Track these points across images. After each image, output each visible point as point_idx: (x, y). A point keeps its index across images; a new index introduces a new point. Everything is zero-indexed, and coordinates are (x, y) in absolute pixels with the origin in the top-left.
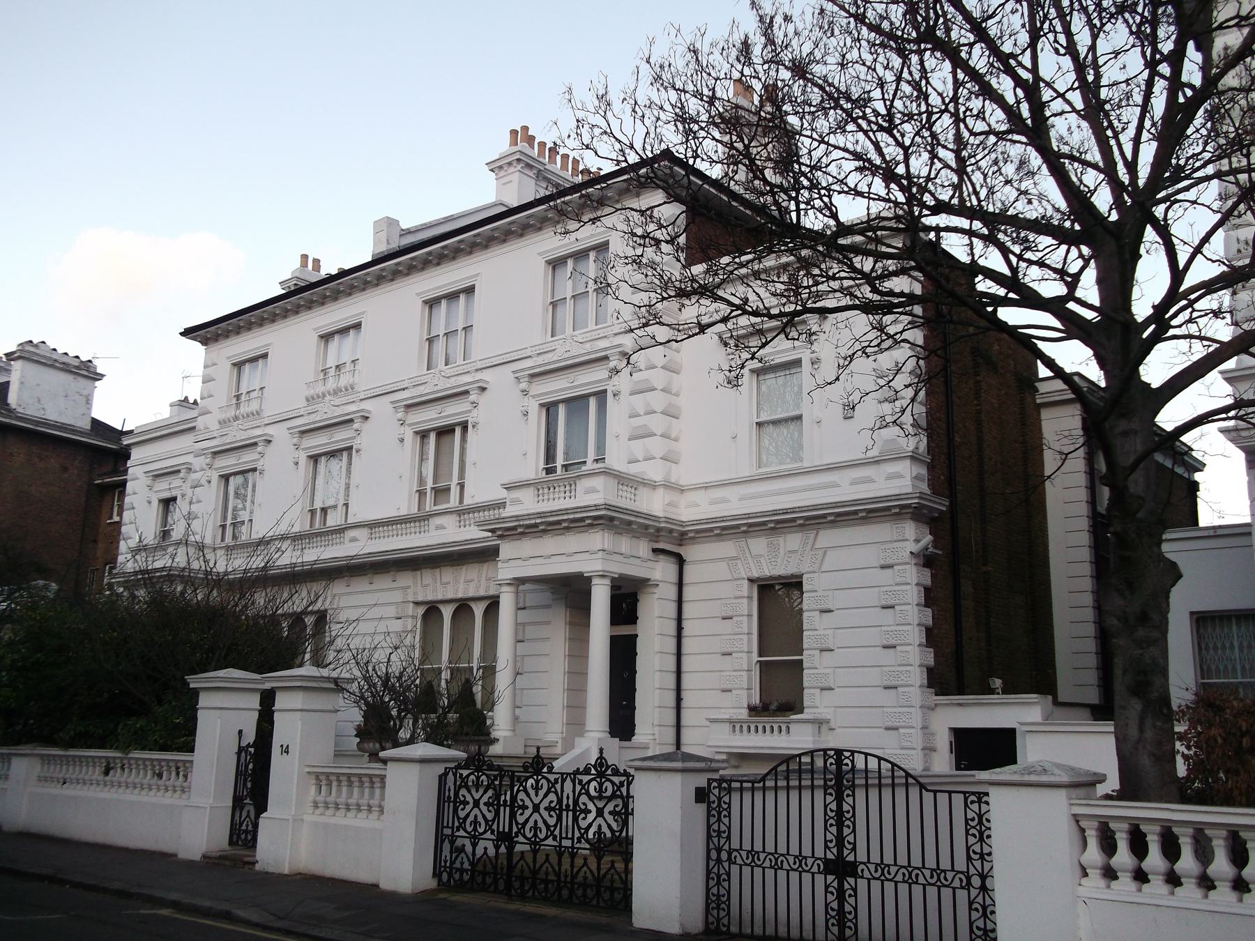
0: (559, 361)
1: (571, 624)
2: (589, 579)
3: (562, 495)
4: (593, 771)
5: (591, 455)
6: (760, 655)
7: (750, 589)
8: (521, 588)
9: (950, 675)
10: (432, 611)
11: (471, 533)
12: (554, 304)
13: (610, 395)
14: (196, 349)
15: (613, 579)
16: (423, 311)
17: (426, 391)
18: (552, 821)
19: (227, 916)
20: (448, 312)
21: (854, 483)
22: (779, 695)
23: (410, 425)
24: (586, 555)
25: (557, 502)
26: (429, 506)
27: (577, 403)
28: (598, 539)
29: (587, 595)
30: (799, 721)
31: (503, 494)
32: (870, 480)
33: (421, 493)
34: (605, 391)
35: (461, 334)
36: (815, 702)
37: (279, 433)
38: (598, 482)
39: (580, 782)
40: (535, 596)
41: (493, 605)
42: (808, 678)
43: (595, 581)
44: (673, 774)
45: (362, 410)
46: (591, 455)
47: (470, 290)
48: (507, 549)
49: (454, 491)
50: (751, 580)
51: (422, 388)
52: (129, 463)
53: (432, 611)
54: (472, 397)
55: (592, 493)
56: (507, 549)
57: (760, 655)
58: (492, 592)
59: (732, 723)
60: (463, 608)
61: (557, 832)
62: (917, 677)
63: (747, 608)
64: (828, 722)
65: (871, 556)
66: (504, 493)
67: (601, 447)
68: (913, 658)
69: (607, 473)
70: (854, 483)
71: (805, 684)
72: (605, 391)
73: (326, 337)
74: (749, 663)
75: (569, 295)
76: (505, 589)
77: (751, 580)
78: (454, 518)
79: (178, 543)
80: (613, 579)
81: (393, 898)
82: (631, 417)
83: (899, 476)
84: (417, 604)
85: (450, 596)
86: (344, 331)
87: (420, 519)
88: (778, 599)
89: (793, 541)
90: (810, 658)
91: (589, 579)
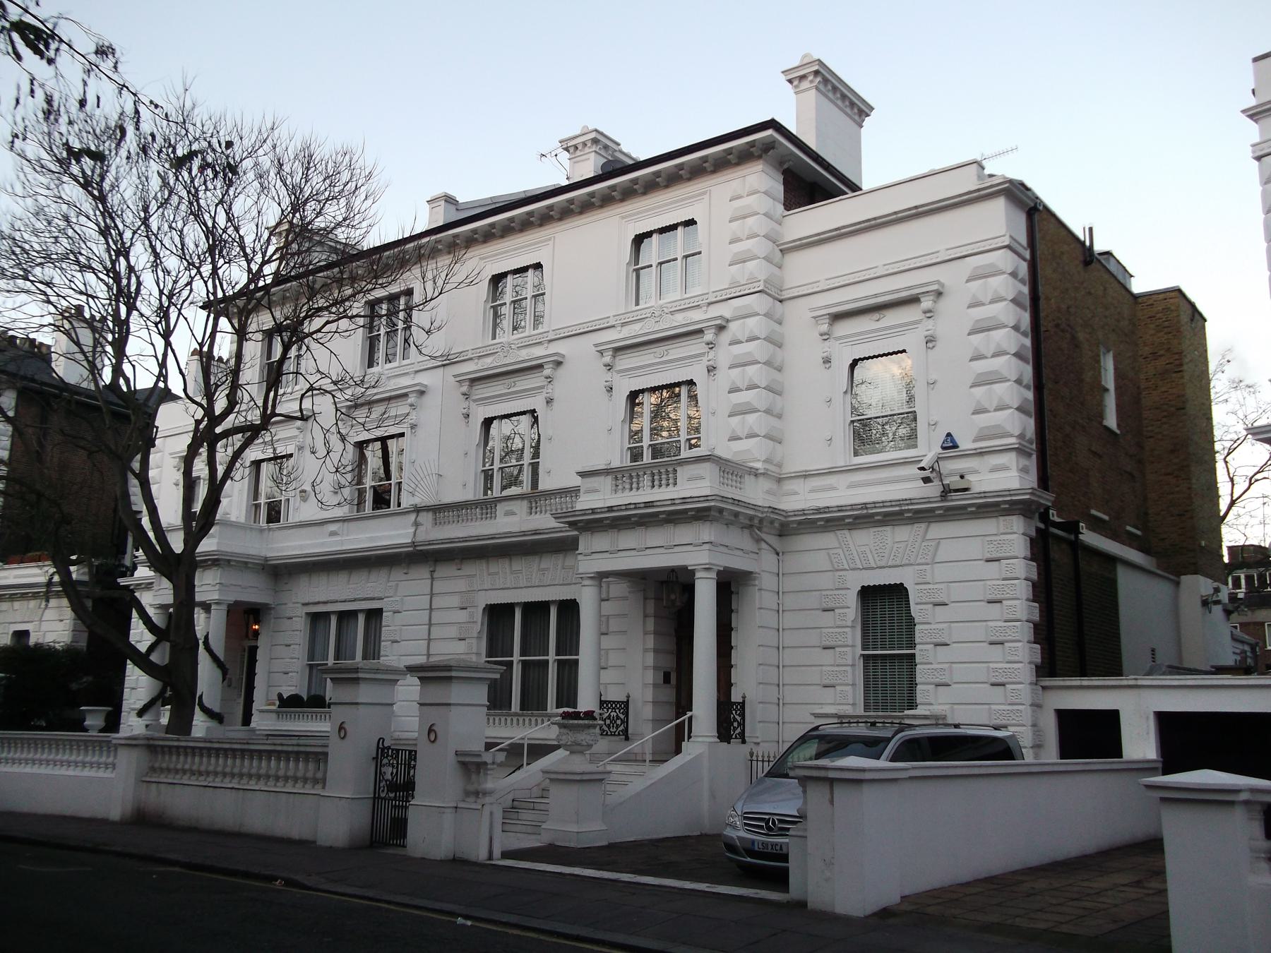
0: (634, 337)
2: (693, 572)
6: (863, 649)
9: (1051, 666)
10: (498, 615)
11: (545, 522)
15: (229, 606)
25: (646, 494)
26: (496, 492)
28: (706, 532)
29: (689, 589)
31: (577, 481)
33: (488, 476)
37: (579, 352)
40: (619, 588)
42: (921, 672)
43: (698, 575)
48: (588, 543)
49: (526, 477)
53: (498, 615)
54: (547, 372)
55: (694, 485)
57: (863, 649)
60: (535, 611)
62: (1025, 672)
65: (975, 548)
66: (577, 481)
68: (1022, 654)
71: (918, 680)
74: (854, 659)
78: (525, 504)
80: (719, 573)
83: (1004, 468)
87: (486, 506)
90: (922, 651)
91: (693, 572)
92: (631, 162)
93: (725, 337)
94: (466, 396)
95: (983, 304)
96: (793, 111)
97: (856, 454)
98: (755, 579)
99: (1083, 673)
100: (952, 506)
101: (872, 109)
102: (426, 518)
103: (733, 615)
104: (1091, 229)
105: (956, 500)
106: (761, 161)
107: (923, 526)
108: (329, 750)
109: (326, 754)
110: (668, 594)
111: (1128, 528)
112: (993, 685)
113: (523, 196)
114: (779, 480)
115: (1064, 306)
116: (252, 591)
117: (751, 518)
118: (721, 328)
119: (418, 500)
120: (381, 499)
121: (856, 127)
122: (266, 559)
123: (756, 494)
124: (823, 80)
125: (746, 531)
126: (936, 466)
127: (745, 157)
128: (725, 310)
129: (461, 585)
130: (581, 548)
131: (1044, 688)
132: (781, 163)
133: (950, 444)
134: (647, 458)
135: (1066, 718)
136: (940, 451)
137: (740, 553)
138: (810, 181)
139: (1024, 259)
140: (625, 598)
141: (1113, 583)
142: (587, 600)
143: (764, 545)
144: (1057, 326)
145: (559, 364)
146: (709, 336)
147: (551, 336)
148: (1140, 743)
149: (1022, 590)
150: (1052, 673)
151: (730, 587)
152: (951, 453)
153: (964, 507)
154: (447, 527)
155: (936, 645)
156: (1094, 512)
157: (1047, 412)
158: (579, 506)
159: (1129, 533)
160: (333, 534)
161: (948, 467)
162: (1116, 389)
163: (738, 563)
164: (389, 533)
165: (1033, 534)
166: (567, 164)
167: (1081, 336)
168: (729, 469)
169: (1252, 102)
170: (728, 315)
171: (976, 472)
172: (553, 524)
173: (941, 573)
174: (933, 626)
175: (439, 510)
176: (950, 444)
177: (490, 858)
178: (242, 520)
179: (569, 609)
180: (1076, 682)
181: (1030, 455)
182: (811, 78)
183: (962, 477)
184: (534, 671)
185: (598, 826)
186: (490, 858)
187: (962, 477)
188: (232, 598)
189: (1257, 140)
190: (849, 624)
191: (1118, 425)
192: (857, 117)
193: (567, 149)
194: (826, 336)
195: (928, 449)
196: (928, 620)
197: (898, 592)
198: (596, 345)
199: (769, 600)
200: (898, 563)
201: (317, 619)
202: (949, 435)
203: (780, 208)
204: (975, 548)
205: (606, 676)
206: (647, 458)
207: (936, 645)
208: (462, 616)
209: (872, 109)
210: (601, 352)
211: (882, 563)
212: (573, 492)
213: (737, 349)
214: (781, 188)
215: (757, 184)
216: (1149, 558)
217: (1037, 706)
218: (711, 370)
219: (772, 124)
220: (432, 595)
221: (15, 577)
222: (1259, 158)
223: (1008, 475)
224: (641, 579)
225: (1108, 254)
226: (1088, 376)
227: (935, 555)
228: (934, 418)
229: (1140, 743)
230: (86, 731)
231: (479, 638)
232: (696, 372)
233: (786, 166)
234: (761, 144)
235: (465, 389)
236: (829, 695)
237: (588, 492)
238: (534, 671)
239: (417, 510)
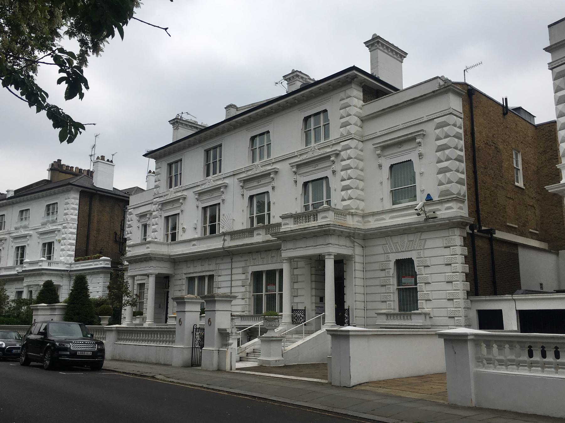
2: (324, 256)
5: (325, 200)
9: (475, 291)
10: (257, 276)
15: (156, 275)
29: (140, 284)
30: (415, 314)
31: (279, 220)
33: (252, 219)
36: (424, 306)
40: (301, 264)
41: (281, 271)
43: (326, 257)
45: (274, 168)
46: (325, 200)
52: (128, 207)
53: (257, 276)
57: (398, 285)
60: (202, 278)
62: (462, 295)
64: (429, 314)
67: (329, 195)
68: (461, 286)
79: (269, 228)
80: (335, 256)
82: (438, 162)
87: (250, 232)
92: (312, 82)
93: (340, 158)
94: (242, 187)
95: (345, 160)
97: (393, 204)
98: (352, 258)
99: (495, 294)
100: (430, 226)
102: (228, 238)
103: (345, 273)
104: (506, 99)
105: (431, 223)
108: (176, 330)
109: (175, 331)
111: (531, 230)
112: (448, 300)
113: (259, 104)
115: (491, 135)
116: (164, 269)
117: (349, 233)
119: (224, 230)
120: (213, 230)
122: (170, 256)
123: (352, 222)
125: (347, 238)
126: (423, 209)
128: (339, 148)
129: (242, 264)
130: (283, 248)
131: (471, 301)
132: (361, 83)
133: (429, 198)
134: (311, 209)
135: (482, 314)
136: (425, 202)
137: (337, 246)
138: (375, 89)
139: (461, 118)
140: (304, 268)
141: (517, 255)
142: (286, 268)
143: (356, 244)
144: (486, 144)
147: (273, 161)
148: (511, 323)
149: (460, 259)
150: (477, 294)
152: (429, 202)
153: (435, 226)
154: (236, 241)
156: (508, 224)
157: (479, 181)
158: (281, 230)
159: (531, 232)
160: (194, 245)
161: (427, 209)
162: (523, 169)
164: (215, 244)
165: (466, 235)
166: (286, 86)
167: (501, 147)
169: (548, 44)
171: (440, 210)
173: (427, 253)
174: (424, 276)
175: (234, 234)
176: (429, 198)
177: (231, 369)
178: (162, 241)
180: (488, 298)
181: (463, 202)
183: (434, 212)
185: (280, 358)
186: (231, 369)
187: (434, 212)
189: (551, 61)
190: (391, 275)
191: (524, 185)
192: (400, 59)
193: (286, 80)
194: (379, 156)
195: (420, 202)
196: (422, 273)
197: (409, 262)
198: (290, 164)
199: (358, 266)
200: (410, 249)
201: (191, 280)
202: (429, 195)
203: (361, 103)
204: (439, 243)
205: (296, 300)
206: (311, 209)
208: (243, 277)
211: (404, 250)
212: (279, 225)
213: (344, 163)
214: (361, 94)
215: (355, 96)
216: (543, 243)
217: (467, 308)
218: (334, 172)
219: (354, 68)
220: (232, 268)
221: (82, 266)
222: (552, 69)
223: (458, 210)
224: (308, 258)
225: (519, 109)
226: (505, 165)
227: (424, 245)
228: (423, 188)
229: (511, 323)
230: (101, 325)
231: (250, 285)
232: (328, 173)
233: (363, 84)
234: (348, 78)
235: (241, 184)
236: (384, 306)
237: (284, 224)
239: (224, 234)
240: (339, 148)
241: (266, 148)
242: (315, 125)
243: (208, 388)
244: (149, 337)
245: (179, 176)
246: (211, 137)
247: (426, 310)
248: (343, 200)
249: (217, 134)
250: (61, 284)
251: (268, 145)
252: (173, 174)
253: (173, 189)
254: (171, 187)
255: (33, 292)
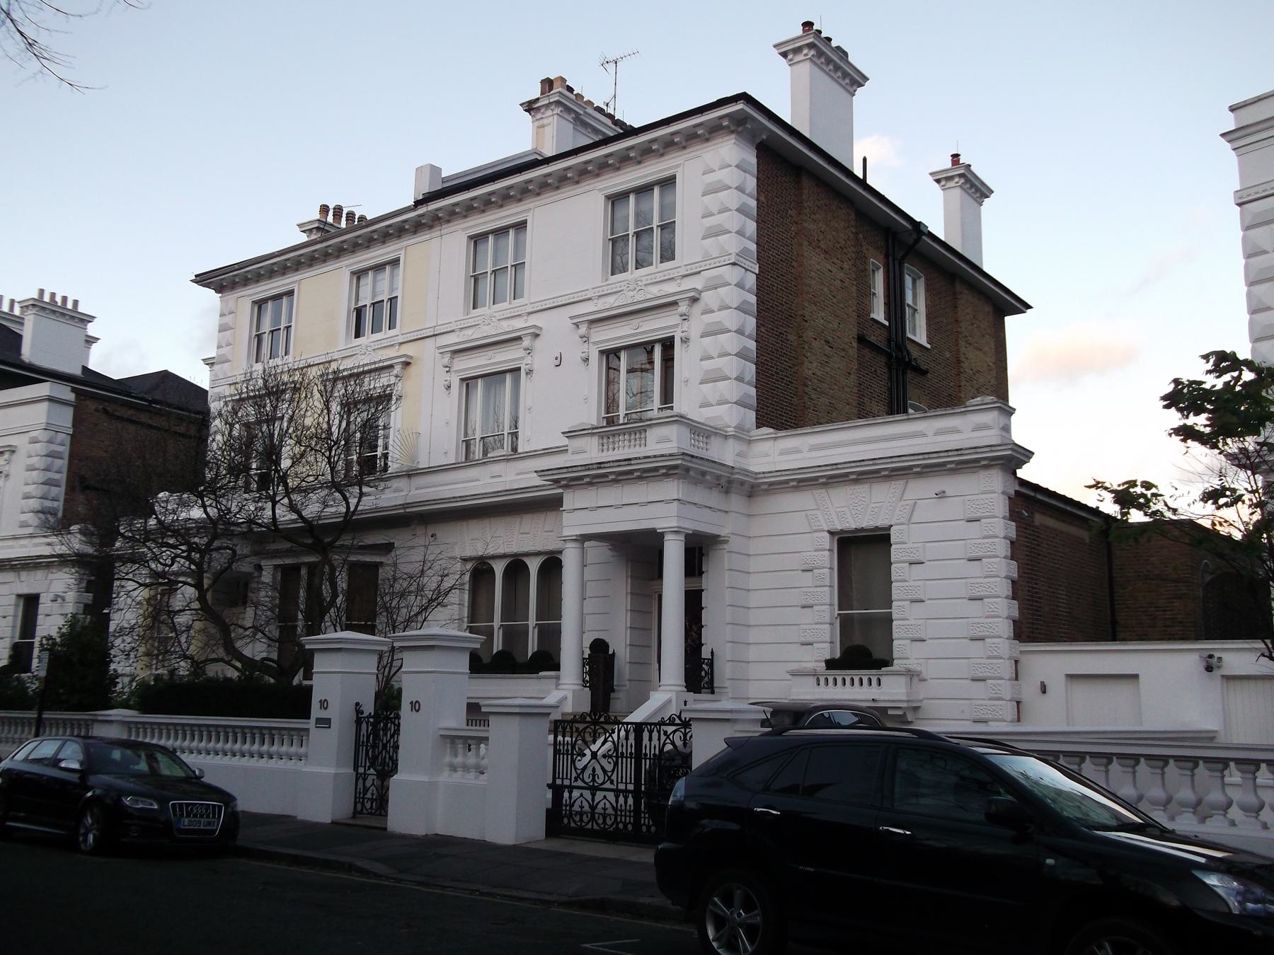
0: (608, 310)
1: (632, 577)
2: (662, 535)
3: (627, 443)
4: (677, 721)
7: (831, 543)
8: (587, 544)
12: (476, 279)
13: (523, 372)
14: (210, 294)
15: (687, 536)
16: (351, 282)
17: (612, 303)
18: (609, 767)
19: (350, 868)
20: (495, 244)
21: (814, 448)
22: (862, 650)
23: (457, 371)
24: (661, 510)
25: (623, 450)
27: (493, 378)
28: (671, 489)
32: (955, 431)
34: (519, 369)
35: (510, 272)
37: (427, 355)
38: (672, 431)
39: (665, 733)
40: (597, 551)
44: (510, 718)
47: (290, 293)
48: (571, 499)
50: (831, 533)
51: (469, 332)
55: (662, 442)
56: (571, 499)
58: (551, 546)
59: (815, 675)
60: (516, 567)
61: (614, 777)
62: (1006, 628)
63: (825, 558)
66: (565, 441)
68: (1001, 611)
69: (681, 420)
70: (814, 448)
71: (895, 635)
72: (519, 369)
73: (359, 275)
75: (489, 270)
76: (570, 545)
77: (831, 533)
80: (687, 536)
81: (323, 825)
84: (465, 560)
85: (501, 551)
86: (379, 268)
88: (862, 552)
89: (40, 574)
90: (898, 609)
91: (662, 535)
93: (697, 309)
96: (782, 92)
101: (866, 79)
106: (733, 136)
107: (902, 482)
110: (639, 552)
114: (750, 442)
118: (694, 300)
121: (848, 96)
124: (819, 53)
127: (714, 130)
128: (696, 282)
130: (567, 505)
145: (407, 364)
146: (683, 308)
151: (698, 552)
155: (914, 640)
163: (705, 524)
168: (699, 431)
170: (699, 287)
172: (538, 481)
179: (552, 565)
182: (805, 51)
184: (514, 606)
188: (691, 526)
207: (914, 640)
209: (866, 79)
210: (577, 325)
213: (709, 318)
219: (745, 97)
234: (742, 116)
238: (514, 606)
240: (696, 282)
241: (282, 334)
242: (636, 226)
243: (490, 894)
244: (23, 731)
245: (282, 334)
246: (646, 152)
247: (912, 664)
248: (705, 405)
249: (669, 145)
250: (723, 532)
251: (390, 299)
252: (266, 327)
253: (368, 339)
254: (357, 335)
255: (45, 606)
